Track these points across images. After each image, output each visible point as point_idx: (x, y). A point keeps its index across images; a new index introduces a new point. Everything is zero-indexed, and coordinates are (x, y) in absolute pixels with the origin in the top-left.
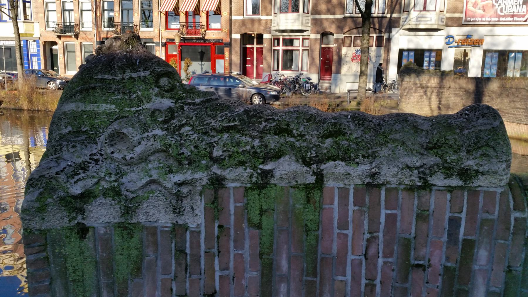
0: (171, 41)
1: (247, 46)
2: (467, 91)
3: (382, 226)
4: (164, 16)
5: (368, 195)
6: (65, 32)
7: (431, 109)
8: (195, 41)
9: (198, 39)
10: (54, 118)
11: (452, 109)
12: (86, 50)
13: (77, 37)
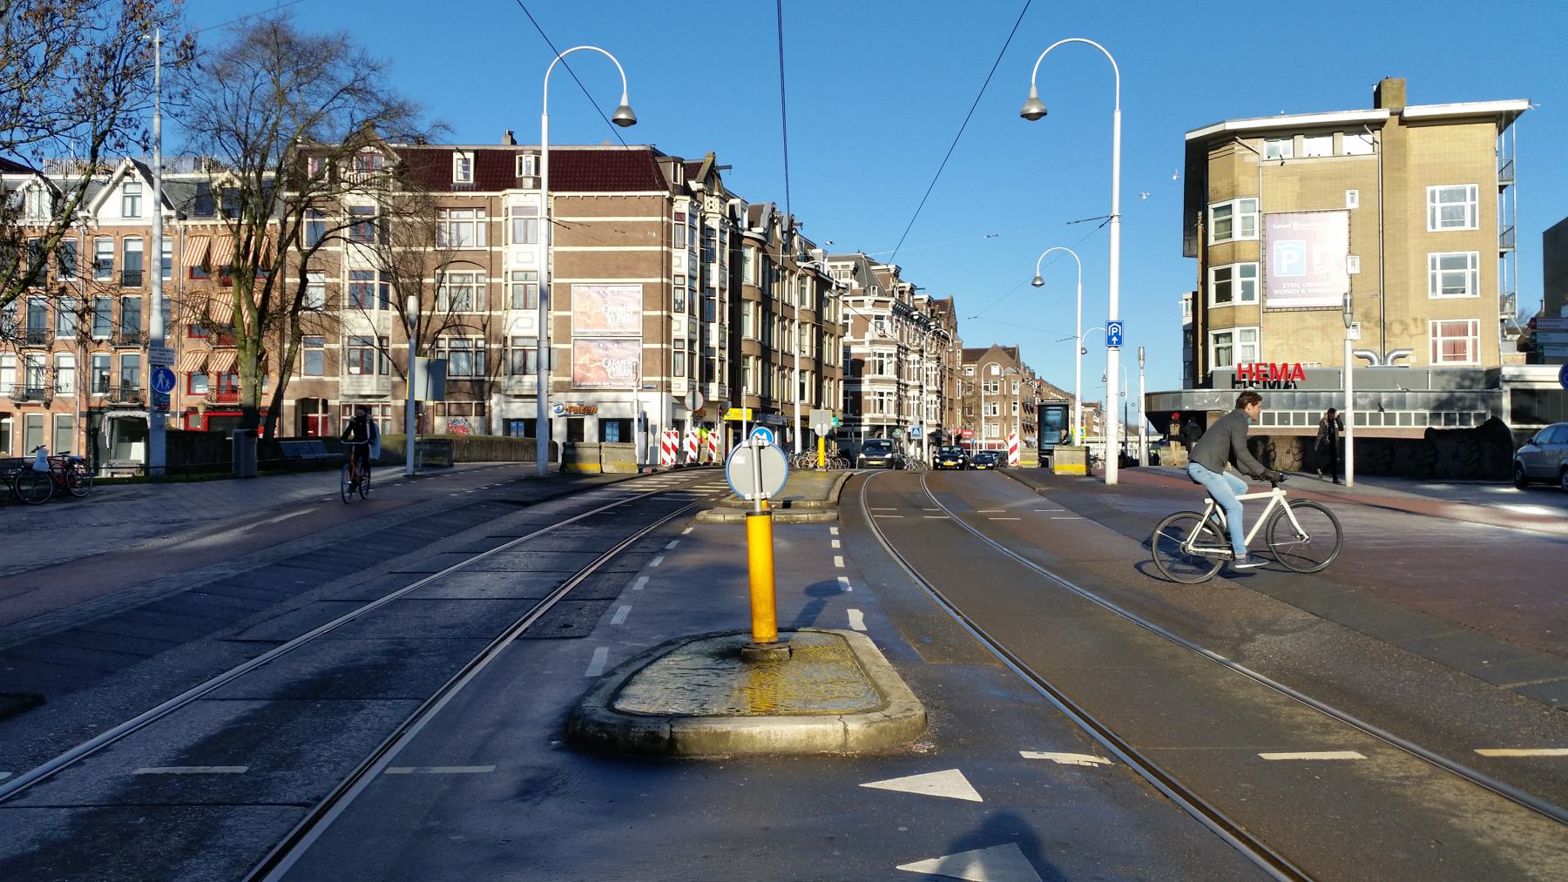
0: (194, 410)
1: (309, 415)
4: (216, 377)
5: (662, 738)
6: (28, 398)
8: (229, 410)
9: (236, 407)
12: (60, 424)
13: (48, 405)
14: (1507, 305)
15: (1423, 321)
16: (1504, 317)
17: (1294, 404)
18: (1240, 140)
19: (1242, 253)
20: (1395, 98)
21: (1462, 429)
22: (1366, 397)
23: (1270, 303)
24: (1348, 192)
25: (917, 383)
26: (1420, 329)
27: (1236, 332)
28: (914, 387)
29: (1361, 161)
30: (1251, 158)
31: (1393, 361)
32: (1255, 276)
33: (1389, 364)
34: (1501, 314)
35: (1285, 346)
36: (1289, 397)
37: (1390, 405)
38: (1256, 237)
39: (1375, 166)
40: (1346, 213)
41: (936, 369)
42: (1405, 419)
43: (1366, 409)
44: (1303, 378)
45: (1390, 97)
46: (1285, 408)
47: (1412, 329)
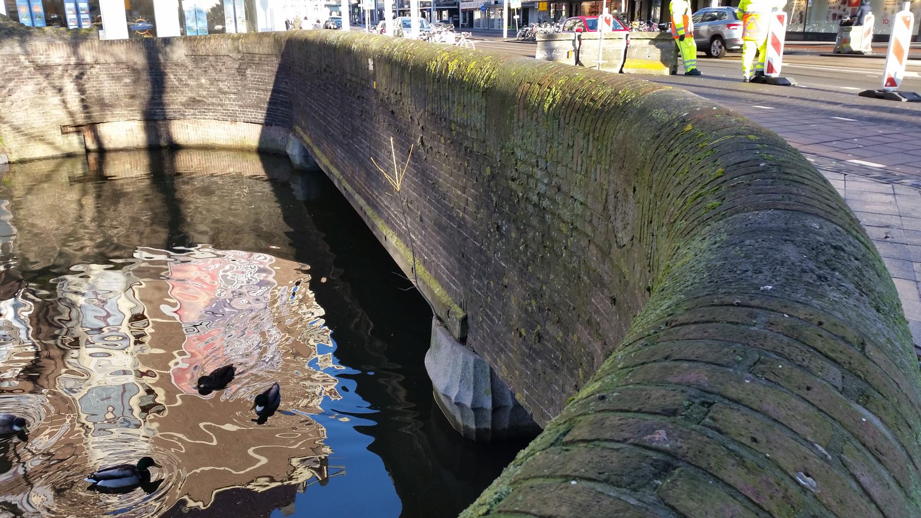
2: (134, 70)
3: (213, 424)
7: (71, 114)
10: (208, 15)
11: (111, 106)
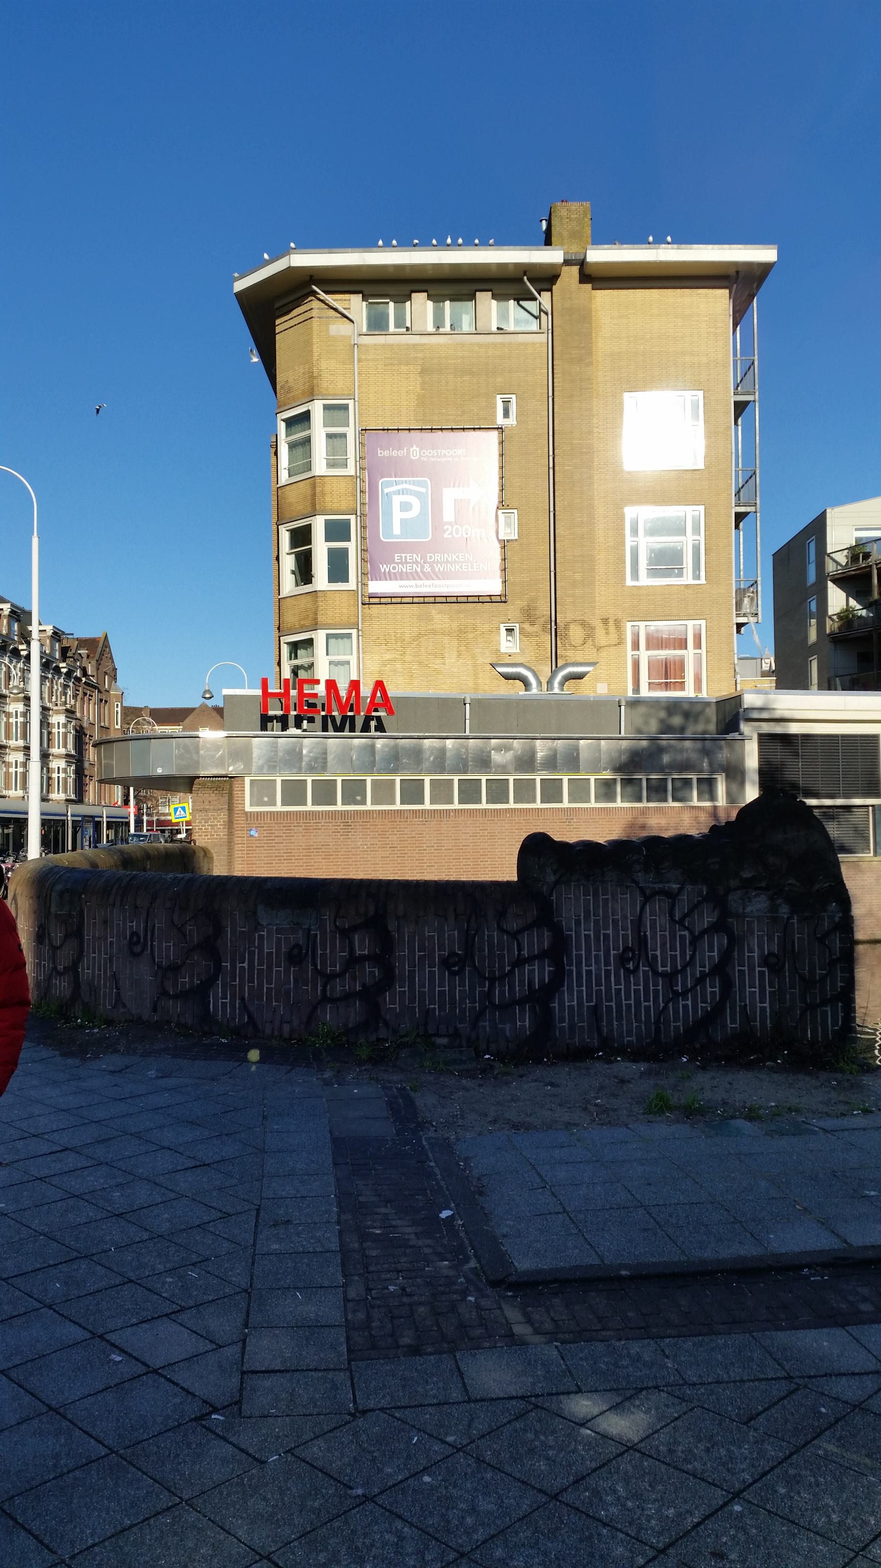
14: (746, 601)
15: (618, 624)
16: (742, 620)
17: (373, 763)
18: (323, 296)
19: (328, 498)
20: (575, 235)
21: (610, 956)
22: (508, 749)
23: (375, 587)
24: (499, 400)
25: (21, 743)
26: (613, 637)
27: (320, 637)
28: (16, 749)
29: (520, 344)
30: (340, 328)
31: (562, 684)
32: (350, 541)
33: (556, 690)
34: (738, 615)
35: (399, 666)
36: (364, 748)
37: (551, 763)
38: (351, 470)
39: (544, 353)
40: (495, 434)
41: (65, 726)
42: (579, 791)
43: (509, 773)
44: (390, 712)
45: (565, 234)
46: (354, 771)
47: (601, 637)
